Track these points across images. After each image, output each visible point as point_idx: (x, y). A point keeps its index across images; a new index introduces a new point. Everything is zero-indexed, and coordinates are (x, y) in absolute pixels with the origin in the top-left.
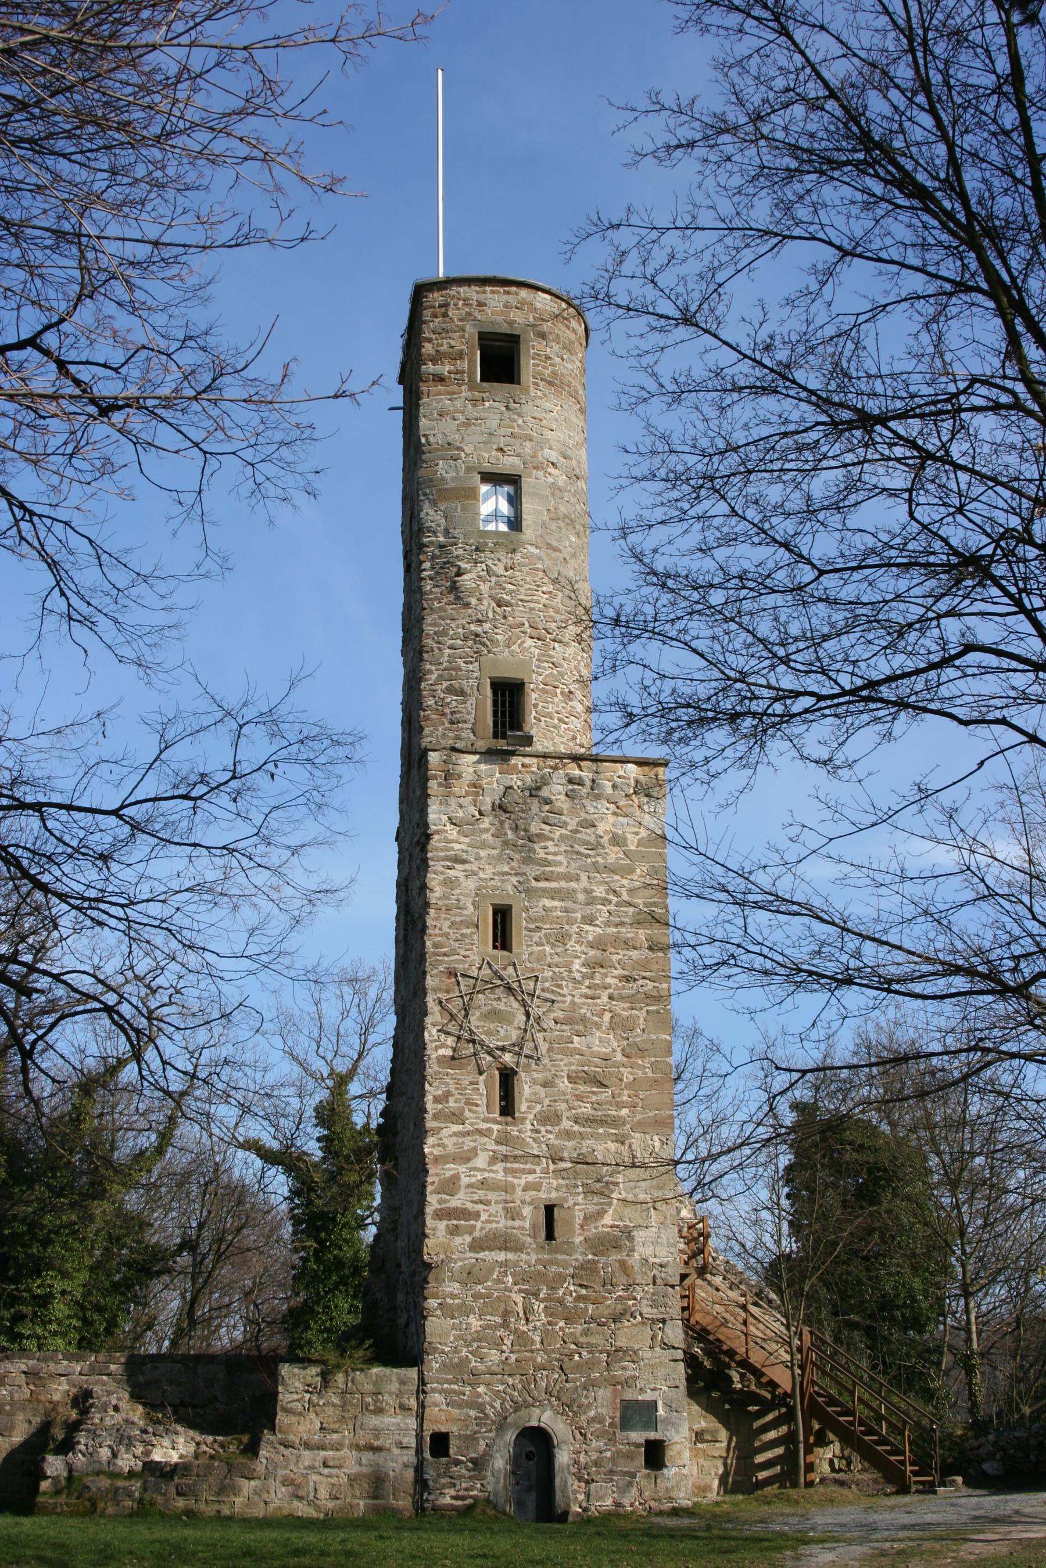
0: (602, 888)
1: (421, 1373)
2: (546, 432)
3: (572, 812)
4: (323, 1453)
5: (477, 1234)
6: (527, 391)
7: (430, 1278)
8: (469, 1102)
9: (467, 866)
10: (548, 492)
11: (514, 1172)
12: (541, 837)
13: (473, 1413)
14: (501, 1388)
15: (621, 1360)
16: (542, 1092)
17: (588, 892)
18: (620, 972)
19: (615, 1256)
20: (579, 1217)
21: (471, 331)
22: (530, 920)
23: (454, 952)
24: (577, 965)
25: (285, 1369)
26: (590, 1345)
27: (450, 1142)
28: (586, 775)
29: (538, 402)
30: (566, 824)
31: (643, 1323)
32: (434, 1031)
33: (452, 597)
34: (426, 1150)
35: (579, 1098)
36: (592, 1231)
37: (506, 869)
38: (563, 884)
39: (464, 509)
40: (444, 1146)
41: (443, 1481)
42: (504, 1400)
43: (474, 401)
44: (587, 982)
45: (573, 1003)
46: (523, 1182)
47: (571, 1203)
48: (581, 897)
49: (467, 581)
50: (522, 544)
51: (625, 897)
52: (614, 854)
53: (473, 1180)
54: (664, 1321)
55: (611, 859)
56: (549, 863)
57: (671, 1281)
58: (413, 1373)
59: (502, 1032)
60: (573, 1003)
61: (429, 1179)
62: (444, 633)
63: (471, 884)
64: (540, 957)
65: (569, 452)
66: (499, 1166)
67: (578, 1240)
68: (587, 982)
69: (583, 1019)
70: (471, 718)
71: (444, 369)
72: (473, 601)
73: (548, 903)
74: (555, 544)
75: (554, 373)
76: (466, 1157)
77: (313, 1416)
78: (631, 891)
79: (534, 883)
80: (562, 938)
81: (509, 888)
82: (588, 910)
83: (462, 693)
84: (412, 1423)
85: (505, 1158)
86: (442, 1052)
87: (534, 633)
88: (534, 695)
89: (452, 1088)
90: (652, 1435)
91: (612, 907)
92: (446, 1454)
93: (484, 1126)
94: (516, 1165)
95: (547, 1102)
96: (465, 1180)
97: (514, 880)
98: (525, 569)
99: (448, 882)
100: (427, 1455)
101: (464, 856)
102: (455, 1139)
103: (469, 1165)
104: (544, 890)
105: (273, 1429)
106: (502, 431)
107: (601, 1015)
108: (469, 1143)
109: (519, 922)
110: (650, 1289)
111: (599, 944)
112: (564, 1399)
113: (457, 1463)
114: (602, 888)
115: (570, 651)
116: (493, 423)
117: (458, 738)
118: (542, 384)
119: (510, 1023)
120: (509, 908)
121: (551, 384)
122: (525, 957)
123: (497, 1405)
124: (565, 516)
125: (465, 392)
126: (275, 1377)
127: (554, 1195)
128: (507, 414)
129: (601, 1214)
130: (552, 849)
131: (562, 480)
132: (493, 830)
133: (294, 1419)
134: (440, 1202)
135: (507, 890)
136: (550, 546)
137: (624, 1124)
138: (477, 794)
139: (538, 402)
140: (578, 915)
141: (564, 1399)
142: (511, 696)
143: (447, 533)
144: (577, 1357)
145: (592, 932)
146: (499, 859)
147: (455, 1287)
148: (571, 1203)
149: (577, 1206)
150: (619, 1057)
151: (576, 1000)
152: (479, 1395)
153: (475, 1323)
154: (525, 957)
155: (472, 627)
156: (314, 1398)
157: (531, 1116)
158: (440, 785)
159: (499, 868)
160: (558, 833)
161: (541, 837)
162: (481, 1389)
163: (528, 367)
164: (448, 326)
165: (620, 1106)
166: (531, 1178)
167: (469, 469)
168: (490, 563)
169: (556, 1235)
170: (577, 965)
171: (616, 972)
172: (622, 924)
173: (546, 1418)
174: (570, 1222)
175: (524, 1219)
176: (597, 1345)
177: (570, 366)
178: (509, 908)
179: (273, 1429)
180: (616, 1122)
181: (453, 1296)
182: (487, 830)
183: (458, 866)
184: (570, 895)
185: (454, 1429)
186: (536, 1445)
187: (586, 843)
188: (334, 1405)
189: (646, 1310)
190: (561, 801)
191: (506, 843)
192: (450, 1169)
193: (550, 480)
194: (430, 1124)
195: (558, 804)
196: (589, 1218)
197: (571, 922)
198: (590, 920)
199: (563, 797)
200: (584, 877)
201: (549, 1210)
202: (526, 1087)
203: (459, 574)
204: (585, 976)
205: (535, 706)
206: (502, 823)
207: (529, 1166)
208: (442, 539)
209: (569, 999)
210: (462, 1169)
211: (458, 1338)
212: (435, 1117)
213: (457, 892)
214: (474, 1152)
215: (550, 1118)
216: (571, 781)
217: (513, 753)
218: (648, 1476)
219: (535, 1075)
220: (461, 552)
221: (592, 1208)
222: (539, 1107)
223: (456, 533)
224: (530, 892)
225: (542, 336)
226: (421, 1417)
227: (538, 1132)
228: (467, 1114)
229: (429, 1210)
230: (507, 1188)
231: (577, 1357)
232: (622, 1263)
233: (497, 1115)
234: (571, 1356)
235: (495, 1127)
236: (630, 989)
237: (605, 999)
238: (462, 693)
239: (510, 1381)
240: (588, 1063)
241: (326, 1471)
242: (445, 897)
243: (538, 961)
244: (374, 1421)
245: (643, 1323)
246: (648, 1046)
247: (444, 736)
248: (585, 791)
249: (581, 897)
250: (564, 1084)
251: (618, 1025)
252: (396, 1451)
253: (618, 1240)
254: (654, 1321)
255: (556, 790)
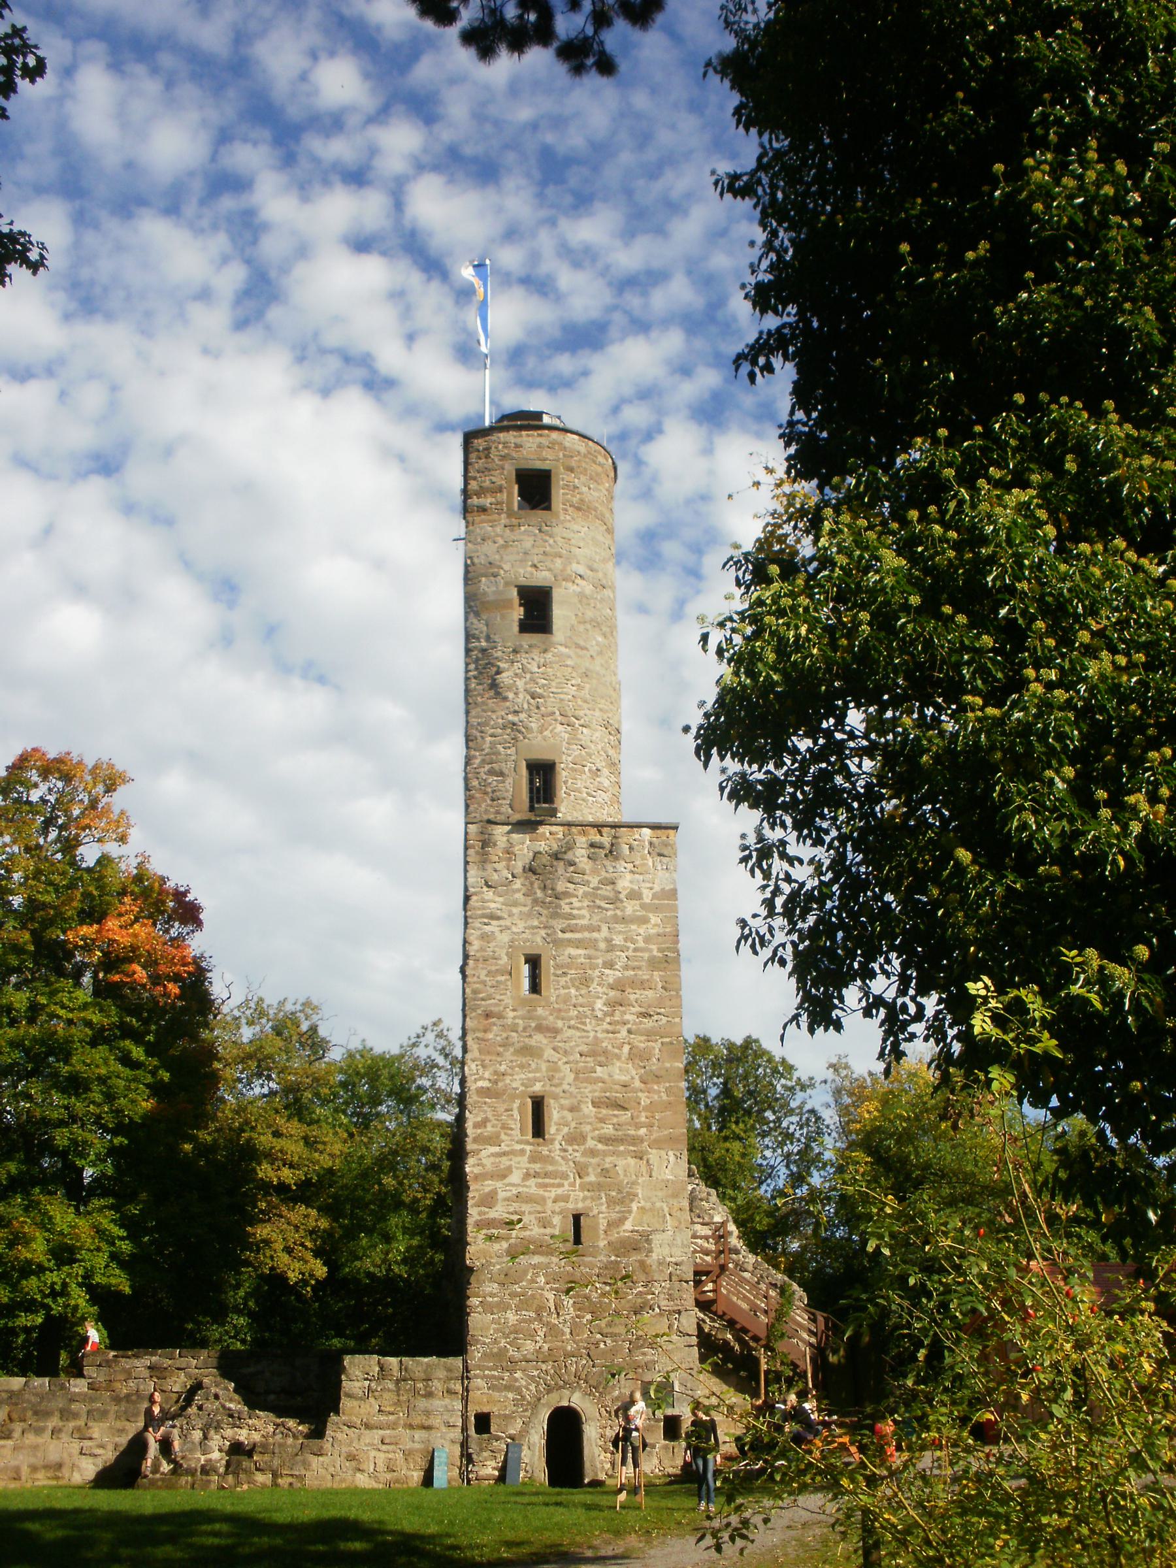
0: (621, 937)
1: (465, 1362)
2: (574, 549)
3: (595, 872)
4: (381, 1432)
5: (512, 1241)
6: (557, 516)
7: (472, 1279)
8: (505, 1127)
9: (502, 922)
10: (576, 600)
11: (545, 1186)
12: (566, 894)
13: (510, 1395)
14: (536, 1373)
15: (642, 1346)
16: (569, 1116)
17: (608, 941)
18: (638, 1009)
19: (635, 1257)
20: (603, 1224)
21: (510, 469)
22: (557, 966)
23: (490, 997)
24: (599, 1004)
25: (347, 1360)
26: (613, 1335)
27: (488, 1162)
28: (606, 840)
29: (567, 525)
30: (588, 882)
31: (661, 1315)
32: (473, 1066)
33: (492, 693)
34: (467, 1170)
35: (602, 1120)
36: (614, 1236)
37: (536, 923)
38: (586, 935)
39: (503, 617)
40: (483, 1166)
41: (485, 1454)
42: (538, 1384)
43: (511, 527)
44: (608, 1019)
45: (596, 1037)
46: (553, 1195)
47: (595, 1212)
48: (602, 945)
49: (505, 678)
50: (553, 645)
51: (641, 944)
52: (630, 908)
53: (509, 1194)
54: (679, 1312)
55: (629, 911)
56: (571, 916)
57: (686, 1277)
58: (457, 1362)
59: (533, 1066)
60: (596, 1037)
61: (470, 1195)
62: (486, 724)
63: (505, 938)
64: (566, 999)
65: (595, 566)
66: (532, 1182)
67: (602, 1243)
68: (608, 1019)
69: (605, 1052)
70: (509, 795)
71: (487, 501)
72: (511, 695)
73: (573, 951)
74: (582, 643)
75: (582, 500)
76: (503, 1175)
77: (372, 1400)
78: (647, 940)
79: (560, 935)
80: (585, 981)
81: (539, 939)
82: (609, 956)
83: (501, 774)
84: (459, 1406)
85: (536, 1175)
86: (480, 1084)
87: (564, 720)
88: (564, 773)
89: (490, 1115)
90: (670, 1412)
91: (630, 953)
92: (488, 1431)
93: (518, 1147)
94: (547, 1181)
95: (573, 1125)
96: (501, 1195)
97: (543, 932)
98: (556, 666)
99: (484, 937)
100: (472, 1431)
101: (499, 913)
102: (492, 1159)
103: (506, 1181)
104: (569, 940)
105: (337, 1413)
106: (536, 551)
107: (620, 1047)
108: (505, 1162)
109: (548, 968)
110: (667, 1284)
111: (619, 986)
112: (591, 1382)
113: (498, 1439)
114: (621, 937)
115: (597, 734)
116: (528, 543)
117: (498, 812)
118: (570, 510)
119: (540, 1056)
120: (539, 956)
121: (579, 509)
122: (553, 999)
123: (533, 1387)
124: (592, 620)
125: (504, 519)
126: (339, 1369)
127: (580, 1205)
128: (540, 535)
129: (622, 1221)
130: (577, 906)
131: (588, 588)
132: (524, 890)
133: (356, 1403)
134: (480, 1214)
135: (537, 942)
136: (578, 646)
137: (642, 1141)
138: (510, 859)
139: (567, 525)
140: (600, 961)
141: (591, 1382)
142: (545, 775)
143: (488, 638)
144: (602, 1345)
145: (611, 975)
146: (529, 915)
147: (494, 1287)
148: (595, 1212)
149: (600, 1214)
150: (637, 1084)
151: (599, 1035)
152: (516, 1380)
153: (512, 1317)
154: (553, 999)
155: (510, 717)
156: (373, 1385)
157: (559, 1138)
158: (477, 853)
159: (529, 923)
160: (581, 890)
161: (566, 894)
162: (518, 1375)
163: (559, 495)
164: (490, 466)
165: (638, 1126)
166: (560, 1191)
167: (507, 584)
168: (525, 661)
169: (583, 1239)
170: (599, 1004)
171: (633, 1010)
172: (639, 968)
173: (576, 1400)
174: (595, 1228)
175: (554, 1227)
176: (620, 1335)
177: (596, 494)
178: (539, 956)
179: (337, 1413)
180: (636, 1141)
181: (492, 1295)
182: (518, 890)
183: (494, 922)
184: (593, 944)
185: (494, 1409)
186: (565, 1429)
187: (604, 898)
188: (389, 1390)
189: (663, 1303)
190: (583, 862)
191: (536, 901)
192: (489, 1185)
193: (578, 589)
194: (470, 1146)
195: (581, 865)
196: (613, 1224)
197: (593, 967)
198: (610, 965)
199: (585, 859)
200: (604, 928)
201: (577, 1218)
202: (555, 1113)
203: (498, 673)
204: (606, 1014)
205: (565, 782)
206: (532, 884)
207: (557, 1181)
208: (484, 644)
209: (592, 1034)
210: (499, 1184)
211: (496, 1331)
212: (475, 1140)
213: (492, 945)
214: (509, 1171)
215: (576, 1138)
216: (592, 845)
217: (541, 823)
218: (666, 1447)
219: (563, 1101)
220: (499, 654)
221: (614, 1216)
222: (566, 1130)
223: (496, 638)
224: (557, 943)
225: (571, 470)
226: (465, 1400)
227: (565, 1151)
228: (503, 1137)
229: (470, 1221)
230: (542, 1201)
231: (602, 1345)
232: (642, 1264)
233: (529, 1137)
234: (597, 1344)
235: (528, 1148)
236: (648, 1023)
237: (624, 1033)
238: (501, 774)
239: (544, 1367)
240: (610, 1090)
241: (384, 1447)
242: (482, 949)
243: (565, 1002)
244: (422, 1403)
245: (661, 1315)
246: (663, 1073)
247: (486, 811)
248: (602, 852)
249: (602, 945)
250: (588, 1109)
251: (638, 1056)
252: (444, 1429)
253: (638, 1244)
254: (671, 1313)
255: (580, 854)
